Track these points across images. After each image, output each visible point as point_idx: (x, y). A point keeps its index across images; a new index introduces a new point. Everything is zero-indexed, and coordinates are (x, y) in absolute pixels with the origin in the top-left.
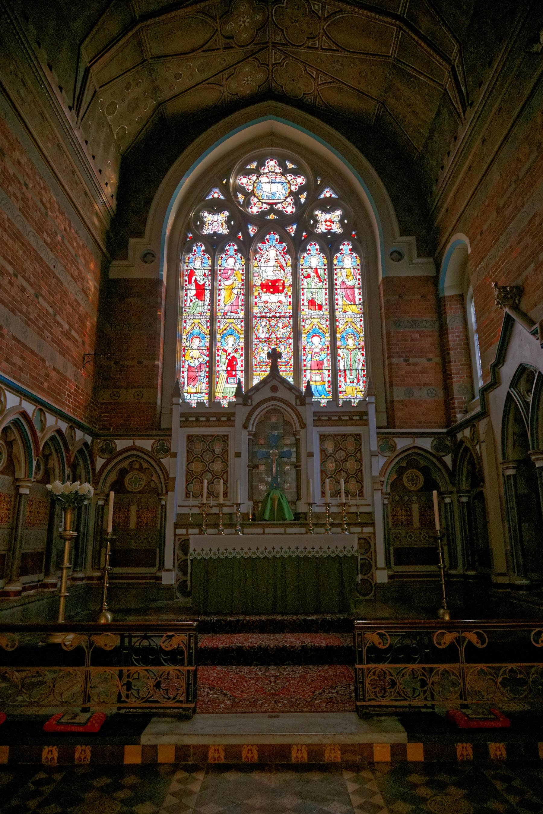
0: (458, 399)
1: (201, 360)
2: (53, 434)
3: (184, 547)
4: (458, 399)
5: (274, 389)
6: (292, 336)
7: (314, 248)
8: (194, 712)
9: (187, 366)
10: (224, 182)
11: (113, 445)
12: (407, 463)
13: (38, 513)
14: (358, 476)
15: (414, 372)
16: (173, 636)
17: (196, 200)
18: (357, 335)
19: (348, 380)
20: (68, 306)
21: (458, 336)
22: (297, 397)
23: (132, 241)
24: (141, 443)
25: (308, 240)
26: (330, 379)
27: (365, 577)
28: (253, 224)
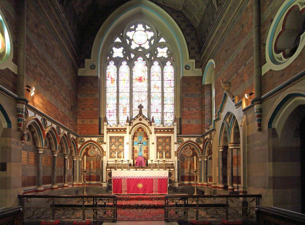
0: (206, 124)
2: (50, 129)
3: (110, 174)
5: (140, 120)
6: (147, 99)
7: (156, 63)
8: (116, 220)
9: (108, 111)
10: (121, 35)
13: (47, 161)
14: (169, 151)
16: (109, 199)
17: (110, 44)
18: (171, 99)
20: (64, 87)
21: (208, 100)
22: (149, 123)
23: (86, 60)
25: (154, 60)
27: (171, 185)
28: (133, 54)
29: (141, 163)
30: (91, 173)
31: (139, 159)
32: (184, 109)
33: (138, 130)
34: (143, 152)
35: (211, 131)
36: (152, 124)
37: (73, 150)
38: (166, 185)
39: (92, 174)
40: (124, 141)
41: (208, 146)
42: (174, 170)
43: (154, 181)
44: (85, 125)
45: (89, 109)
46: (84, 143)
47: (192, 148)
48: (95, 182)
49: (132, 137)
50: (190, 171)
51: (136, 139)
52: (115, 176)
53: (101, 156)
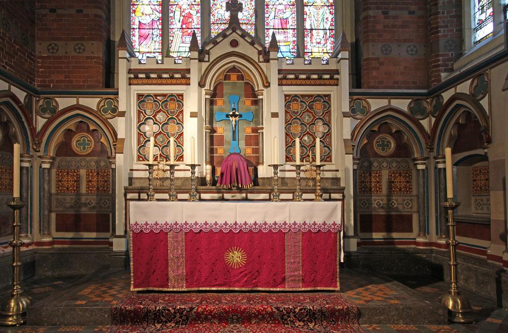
0: (442, 55)
1: (153, 17)
4: (442, 55)
5: (234, 43)
9: (137, 23)
11: (54, 104)
12: (379, 127)
15: (394, 26)
19: (314, 41)
22: (260, 53)
24: (85, 101)
26: (295, 39)
29: (233, 177)
30: (80, 207)
31: (230, 163)
32: (371, 13)
33: (227, 77)
34: (242, 144)
35: (440, 90)
36: (271, 57)
37: (15, 132)
38: (334, 253)
39: (84, 210)
40: (185, 108)
41: (457, 123)
42: (344, 196)
43: (288, 243)
44: (60, 58)
45: (73, 11)
46: (55, 113)
47: (394, 130)
48: (93, 235)
49: (208, 97)
50: (389, 200)
51: (219, 102)
52: (142, 221)
53: (109, 155)
